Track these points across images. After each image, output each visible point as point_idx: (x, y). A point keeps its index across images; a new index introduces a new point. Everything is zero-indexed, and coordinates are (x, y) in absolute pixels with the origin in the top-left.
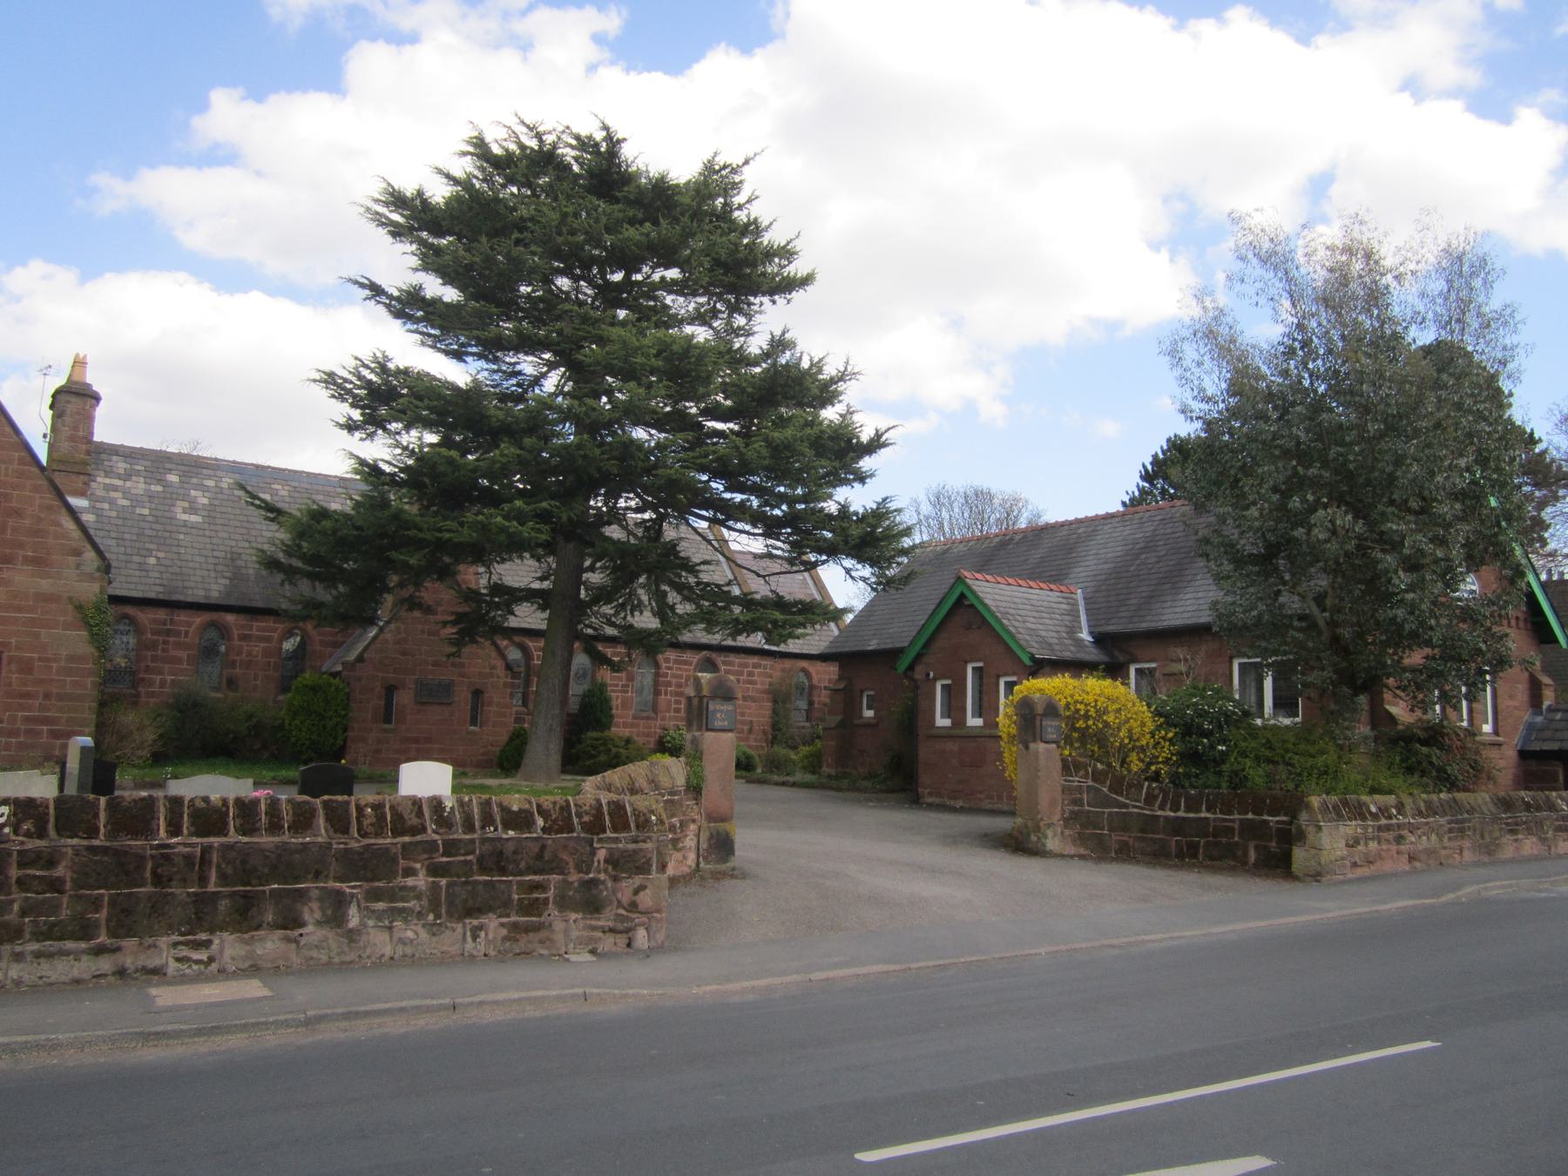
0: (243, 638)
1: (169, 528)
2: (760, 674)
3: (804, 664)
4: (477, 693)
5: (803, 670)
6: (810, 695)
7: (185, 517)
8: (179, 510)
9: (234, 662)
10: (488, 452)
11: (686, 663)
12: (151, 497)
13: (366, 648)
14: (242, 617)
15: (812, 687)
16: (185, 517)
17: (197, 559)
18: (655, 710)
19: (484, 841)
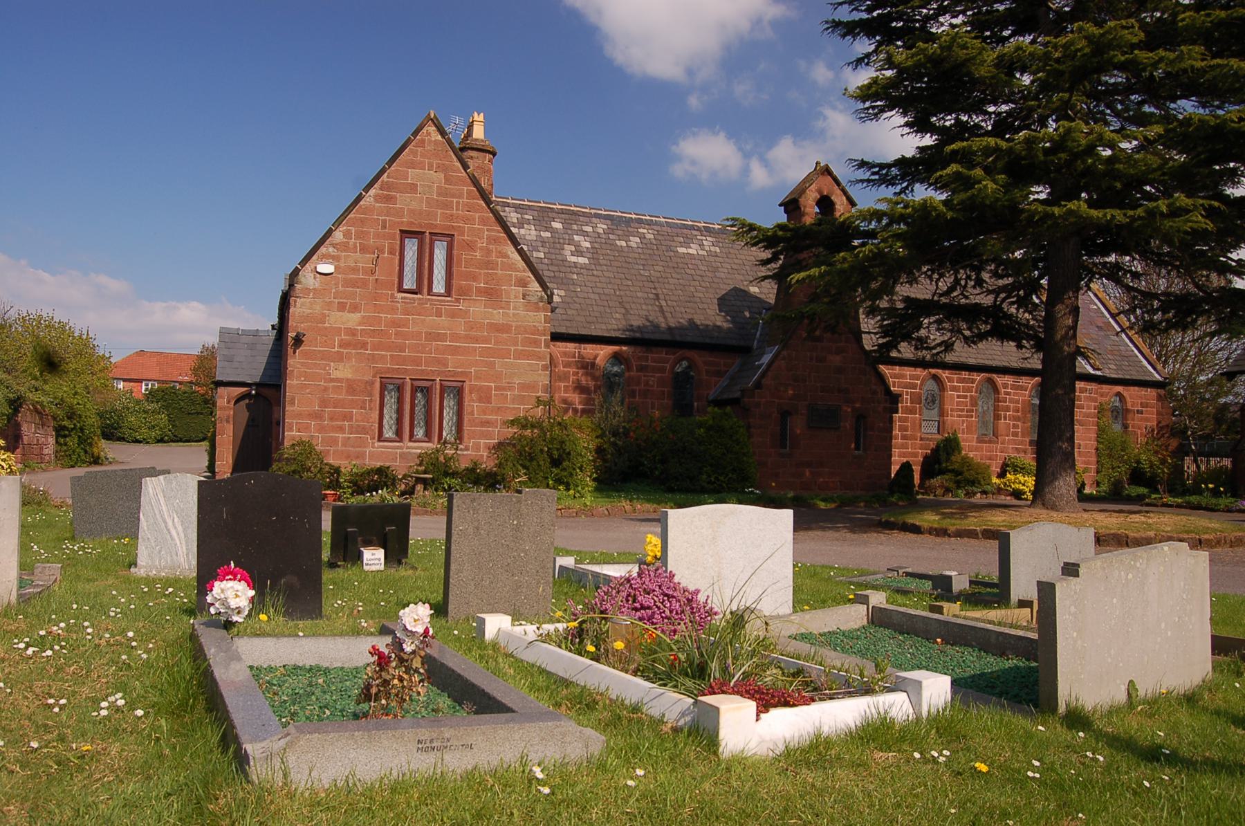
1: (563, 269)
2: (1087, 398)
3: (1119, 389)
5: (1118, 394)
6: (1125, 418)
7: (574, 259)
8: (568, 253)
11: (1022, 388)
12: (544, 242)
13: (763, 375)
14: (639, 349)
15: (1127, 411)
16: (574, 259)
17: (592, 296)
18: (995, 435)
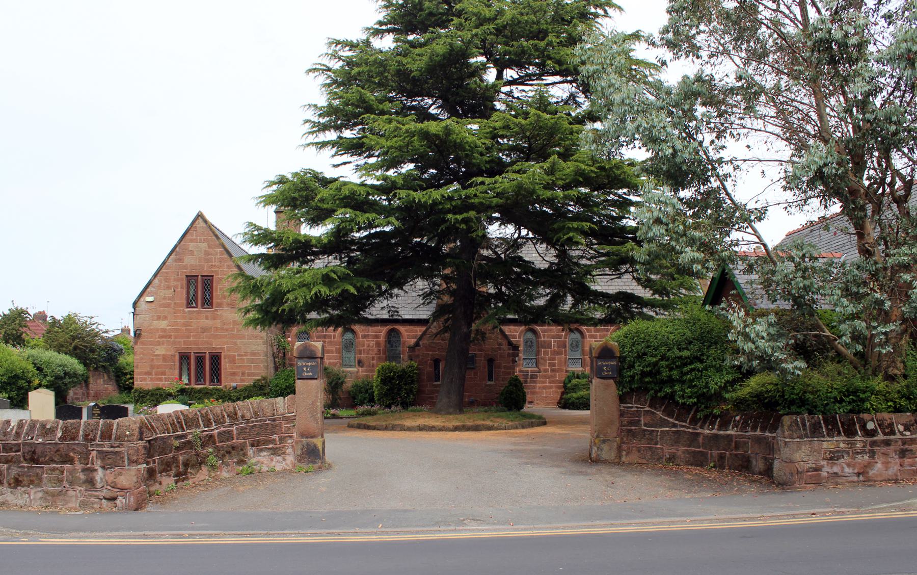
0: (365, 337)
4: (491, 361)
9: (360, 351)
10: (387, 170)
19: (24, 444)
